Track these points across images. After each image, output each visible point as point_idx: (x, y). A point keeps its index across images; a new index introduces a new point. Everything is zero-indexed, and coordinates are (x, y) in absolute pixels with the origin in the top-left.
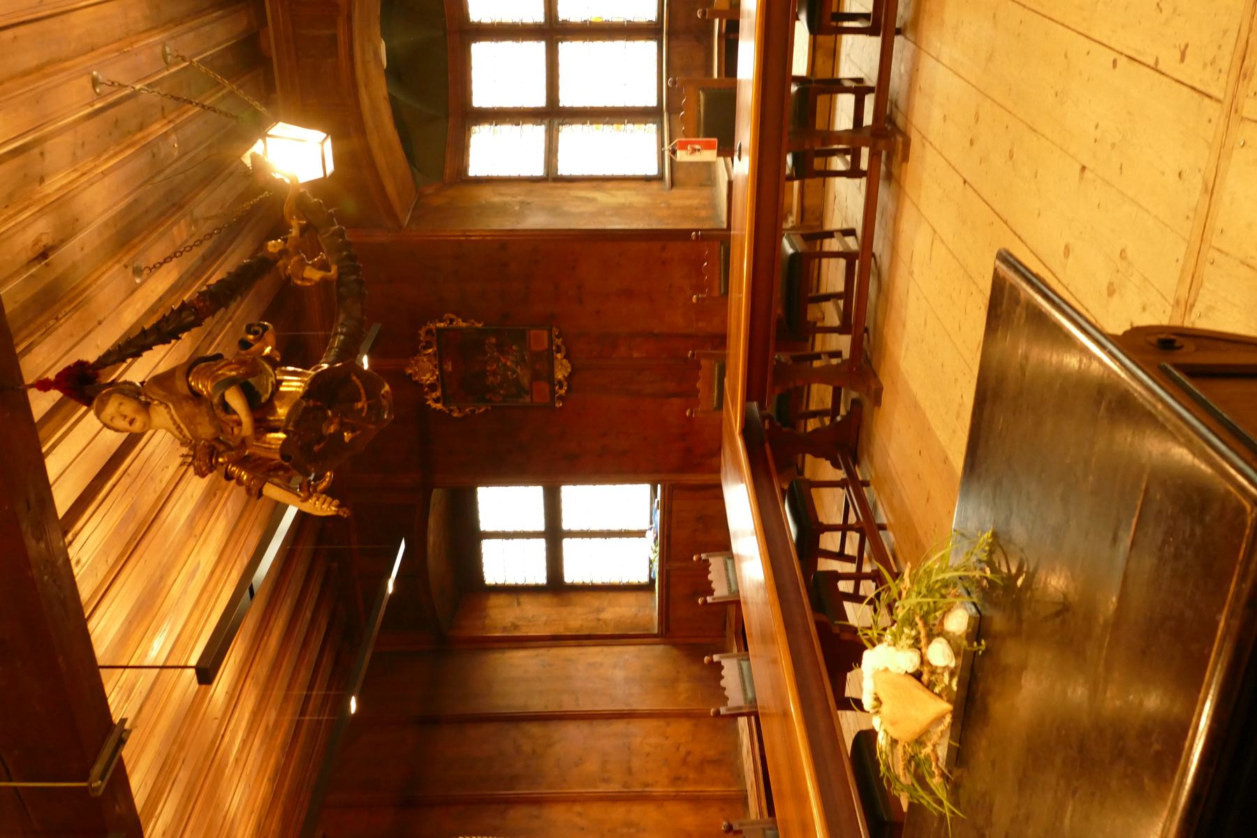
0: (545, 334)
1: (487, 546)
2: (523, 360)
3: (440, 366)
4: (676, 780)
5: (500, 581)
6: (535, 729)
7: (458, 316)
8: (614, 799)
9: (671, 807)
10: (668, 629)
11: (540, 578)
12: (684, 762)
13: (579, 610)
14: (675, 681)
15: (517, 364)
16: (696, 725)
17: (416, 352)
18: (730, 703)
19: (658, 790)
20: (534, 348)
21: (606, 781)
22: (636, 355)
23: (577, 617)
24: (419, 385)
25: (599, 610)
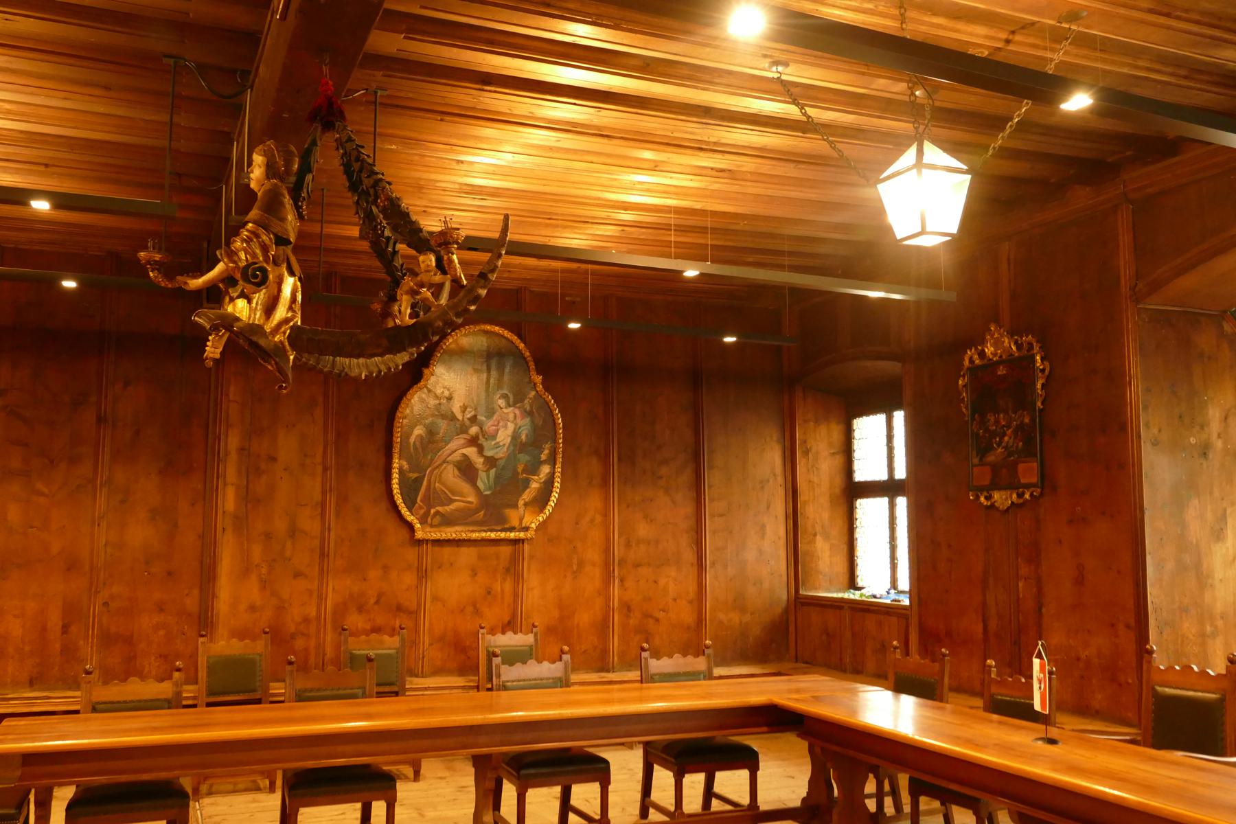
0: (1034, 480)
1: (881, 418)
2: (1010, 455)
3: (1001, 362)
4: (627, 608)
5: (857, 434)
6: (686, 477)
7: (1048, 379)
8: (607, 550)
9: (599, 603)
10: (803, 604)
11: (859, 476)
12: (647, 616)
13: (826, 515)
14: (743, 610)
15: (1006, 448)
16: (688, 628)
17: (1011, 334)
18: (504, 668)
19: (616, 591)
20: (1021, 467)
21: (628, 545)
22: (1021, 585)
23: (818, 509)
24: (983, 342)
25: (827, 537)
